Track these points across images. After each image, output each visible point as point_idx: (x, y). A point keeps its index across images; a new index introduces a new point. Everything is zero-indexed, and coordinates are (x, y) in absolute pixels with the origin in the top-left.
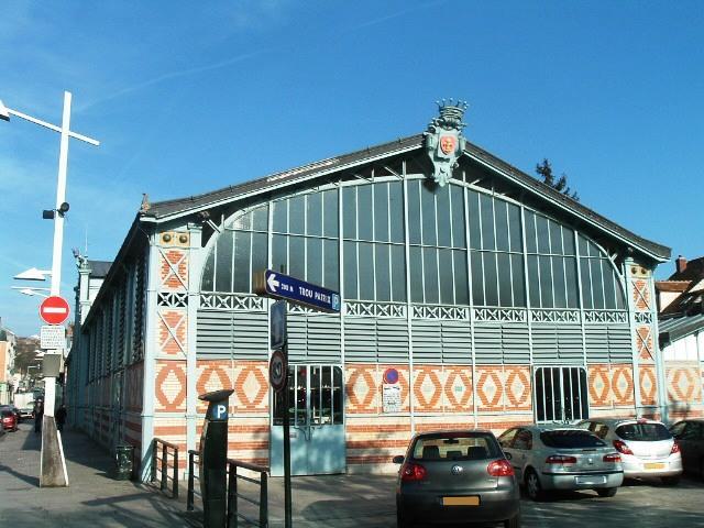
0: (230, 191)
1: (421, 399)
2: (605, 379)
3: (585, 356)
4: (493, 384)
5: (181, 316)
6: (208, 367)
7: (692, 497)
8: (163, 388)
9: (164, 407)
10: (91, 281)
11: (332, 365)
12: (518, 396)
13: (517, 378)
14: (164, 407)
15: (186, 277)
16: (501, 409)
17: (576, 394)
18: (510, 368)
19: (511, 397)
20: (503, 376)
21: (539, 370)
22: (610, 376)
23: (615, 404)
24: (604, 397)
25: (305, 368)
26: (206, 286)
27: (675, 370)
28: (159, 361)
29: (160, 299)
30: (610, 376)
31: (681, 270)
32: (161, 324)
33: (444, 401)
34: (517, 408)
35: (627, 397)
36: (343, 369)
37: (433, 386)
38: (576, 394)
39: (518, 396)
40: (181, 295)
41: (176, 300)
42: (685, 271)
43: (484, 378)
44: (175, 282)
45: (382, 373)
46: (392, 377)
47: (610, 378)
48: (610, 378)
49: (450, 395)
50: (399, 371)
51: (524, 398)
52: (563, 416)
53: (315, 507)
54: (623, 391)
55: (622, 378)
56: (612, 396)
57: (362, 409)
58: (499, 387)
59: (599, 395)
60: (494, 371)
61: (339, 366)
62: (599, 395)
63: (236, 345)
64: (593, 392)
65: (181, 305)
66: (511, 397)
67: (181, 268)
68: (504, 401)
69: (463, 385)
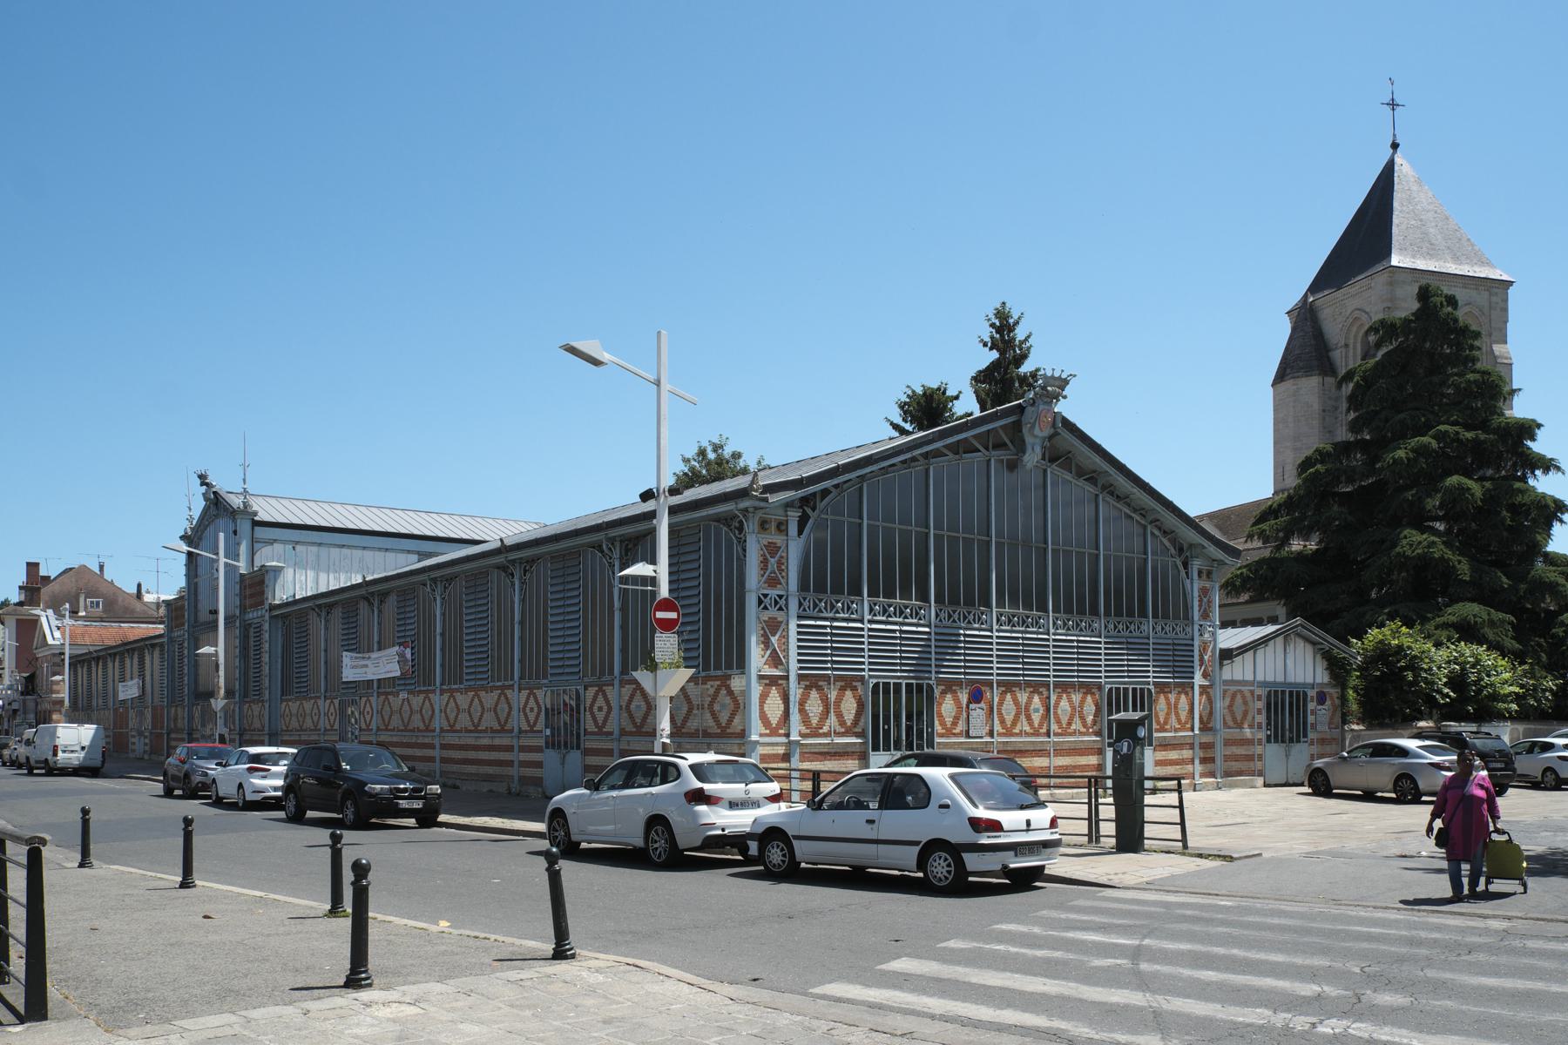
2: (840, 716)
3: (1151, 658)
4: (728, 700)
5: (781, 622)
7: (1112, 998)
8: (766, 708)
9: (768, 731)
10: (256, 528)
11: (881, 681)
14: (768, 731)
15: (784, 574)
21: (876, 685)
24: (1166, 723)
25: (1128, 689)
26: (804, 586)
27: (1231, 692)
28: (761, 677)
29: (760, 602)
32: (762, 632)
35: (1186, 723)
36: (934, 687)
40: (780, 597)
41: (776, 602)
43: (1059, 698)
44: (773, 582)
47: (833, 717)
48: (833, 717)
53: (1488, 719)
56: (1173, 721)
58: (1073, 708)
61: (931, 682)
65: (781, 609)
67: (779, 563)
68: (1173, 721)
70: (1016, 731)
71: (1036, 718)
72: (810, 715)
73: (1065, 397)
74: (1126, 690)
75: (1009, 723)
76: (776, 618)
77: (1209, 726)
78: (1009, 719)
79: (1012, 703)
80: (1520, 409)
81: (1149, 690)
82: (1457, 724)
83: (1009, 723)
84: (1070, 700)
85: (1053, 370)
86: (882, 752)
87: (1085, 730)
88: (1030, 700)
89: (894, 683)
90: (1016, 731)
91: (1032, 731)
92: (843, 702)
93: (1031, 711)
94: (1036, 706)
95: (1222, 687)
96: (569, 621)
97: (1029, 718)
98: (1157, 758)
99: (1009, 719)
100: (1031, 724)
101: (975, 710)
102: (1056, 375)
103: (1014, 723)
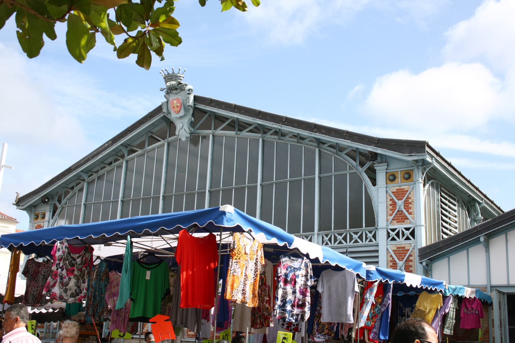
40: (407, 229)
73: (162, 90)
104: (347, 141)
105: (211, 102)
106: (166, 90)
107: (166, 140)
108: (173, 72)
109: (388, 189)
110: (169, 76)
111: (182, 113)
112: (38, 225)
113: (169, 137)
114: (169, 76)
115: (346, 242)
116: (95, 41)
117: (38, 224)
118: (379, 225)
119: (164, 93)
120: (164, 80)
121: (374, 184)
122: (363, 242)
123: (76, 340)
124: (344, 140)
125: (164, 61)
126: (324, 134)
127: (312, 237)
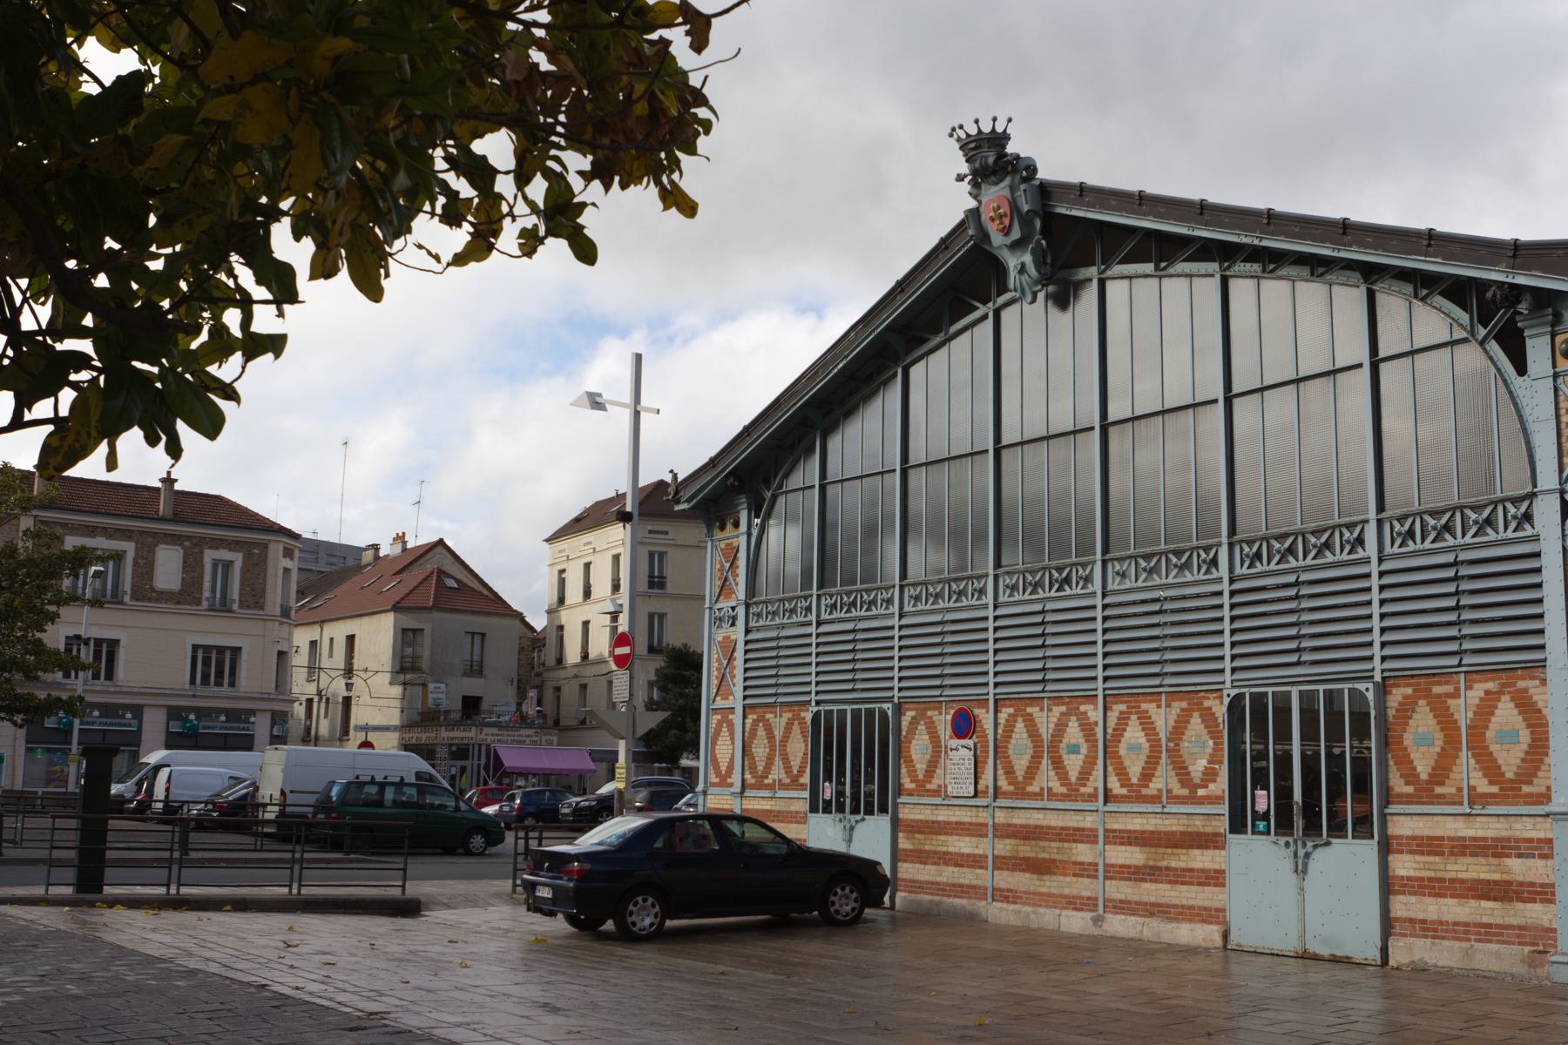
0: (1202, 211)
1: (1491, 770)
6: (1184, 705)
11: (835, 708)
12: (1198, 767)
13: (1196, 722)
16: (1038, 795)
17: (870, 763)
18: (1058, 700)
19: (1181, 770)
20: (1163, 718)
22: (1462, 710)
23: (1475, 798)
30: (1462, 710)
31: (270, 297)
33: (1467, 773)
34: (1193, 799)
37: (1439, 736)
38: (870, 763)
39: (1198, 767)
42: (270, 289)
45: (949, 717)
46: (964, 726)
47: (1463, 718)
48: (1463, 718)
49: (1058, 764)
50: (976, 711)
51: (1210, 775)
52: (1299, 823)
54: (1510, 759)
55: (1506, 712)
56: (1467, 773)
57: (1426, 793)
59: (1423, 770)
60: (1144, 706)
61: (1361, 686)
62: (1423, 770)
63: (1155, 657)
64: (1405, 761)
66: (1181, 770)
69: (1081, 740)
70: (1034, 788)
71: (1073, 764)
72: (757, 759)
73: (960, 178)
74: (842, 713)
75: (1020, 774)
76: (729, 637)
77: (729, 780)
78: (1021, 764)
79: (1025, 736)
80: (689, 39)
81: (883, 714)
82: (83, 771)
83: (1020, 774)
84: (1148, 726)
85: (977, 122)
86: (820, 814)
87: (1185, 792)
88: (1061, 727)
89: (1273, 692)
90: (1034, 788)
91: (1064, 790)
92: (790, 740)
93: (1063, 753)
94: (1074, 741)
95: (1295, 692)
96: (1291, 612)
97: (1058, 764)
98: (1223, 852)
99: (1021, 764)
100: (1063, 776)
101: (957, 749)
102: (987, 129)
103: (1147, 776)
104: (1433, 259)
105: (1347, 231)
106: (970, 178)
107: (990, 305)
108: (980, 132)
109: (1560, 380)
110: (971, 142)
111: (1016, 234)
112: (727, 545)
113: (998, 296)
114: (971, 142)
115: (1044, 592)
116: (675, 58)
117: (727, 541)
118: (1539, 485)
119: (965, 186)
120: (961, 153)
121: (1521, 369)
122: (1334, 555)
123: (439, 897)
124: (1423, 258)
125: (696, 55)
126: (1371, 248)
127: (1363, 528)
